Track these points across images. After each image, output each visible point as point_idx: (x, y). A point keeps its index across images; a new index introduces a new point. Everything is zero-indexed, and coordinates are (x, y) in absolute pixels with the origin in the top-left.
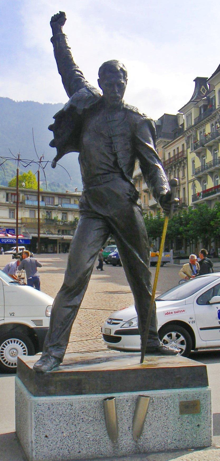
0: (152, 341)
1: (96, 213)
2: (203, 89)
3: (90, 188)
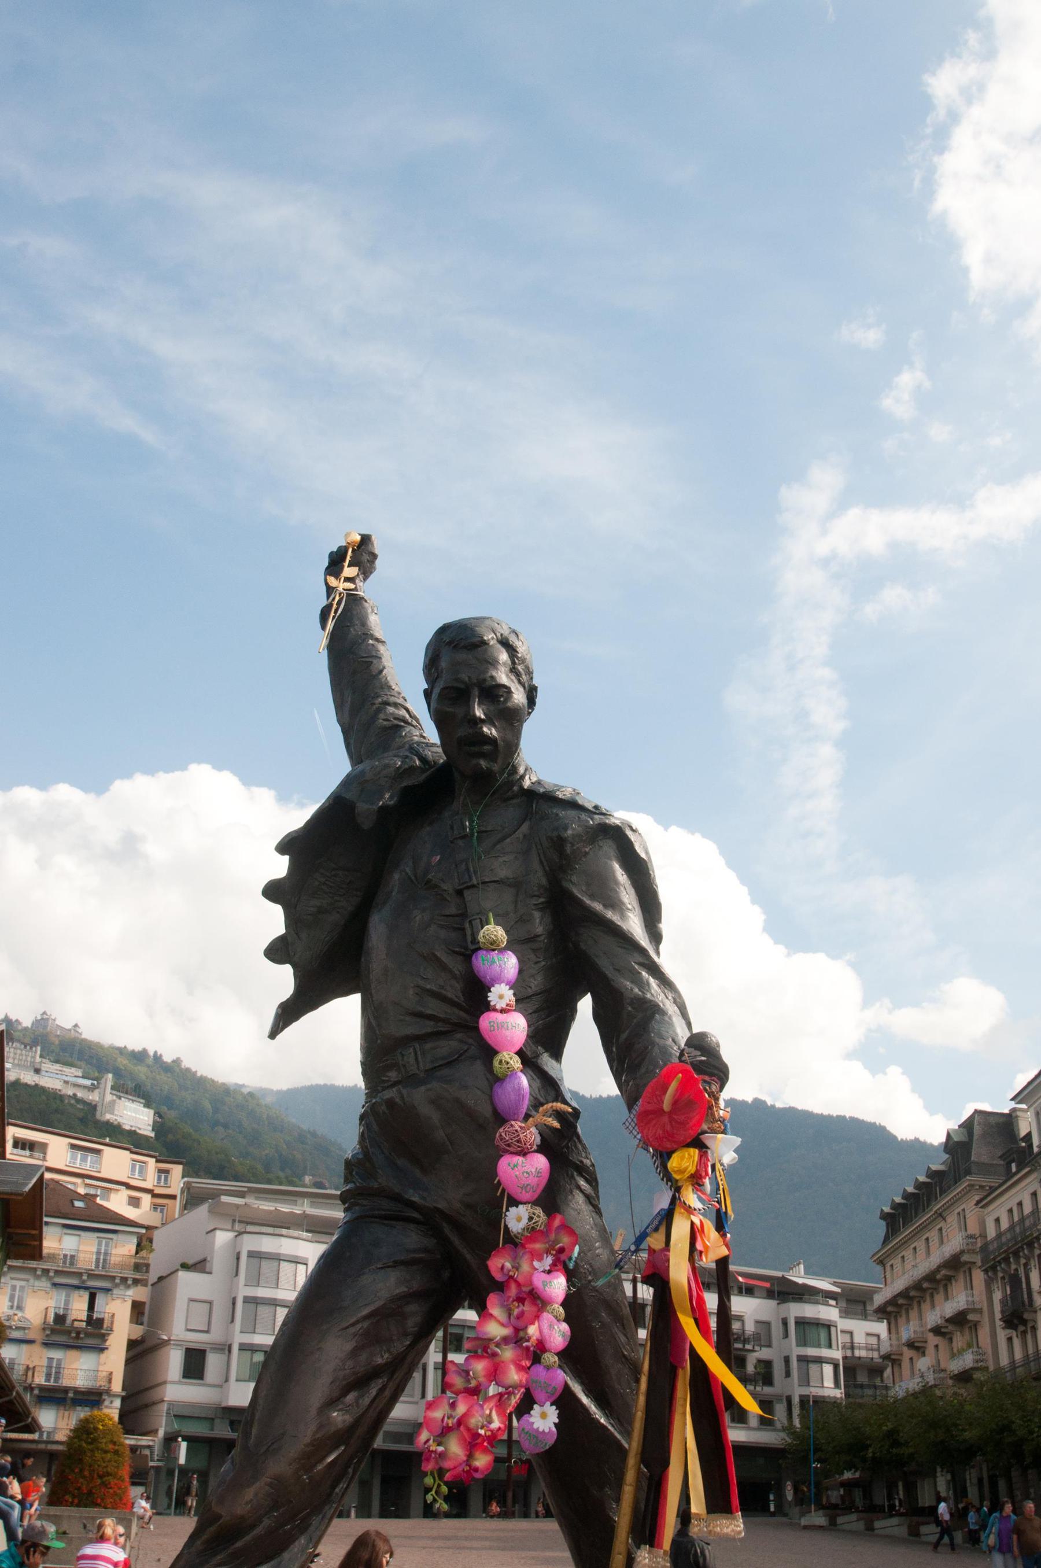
1: (397, 1198)
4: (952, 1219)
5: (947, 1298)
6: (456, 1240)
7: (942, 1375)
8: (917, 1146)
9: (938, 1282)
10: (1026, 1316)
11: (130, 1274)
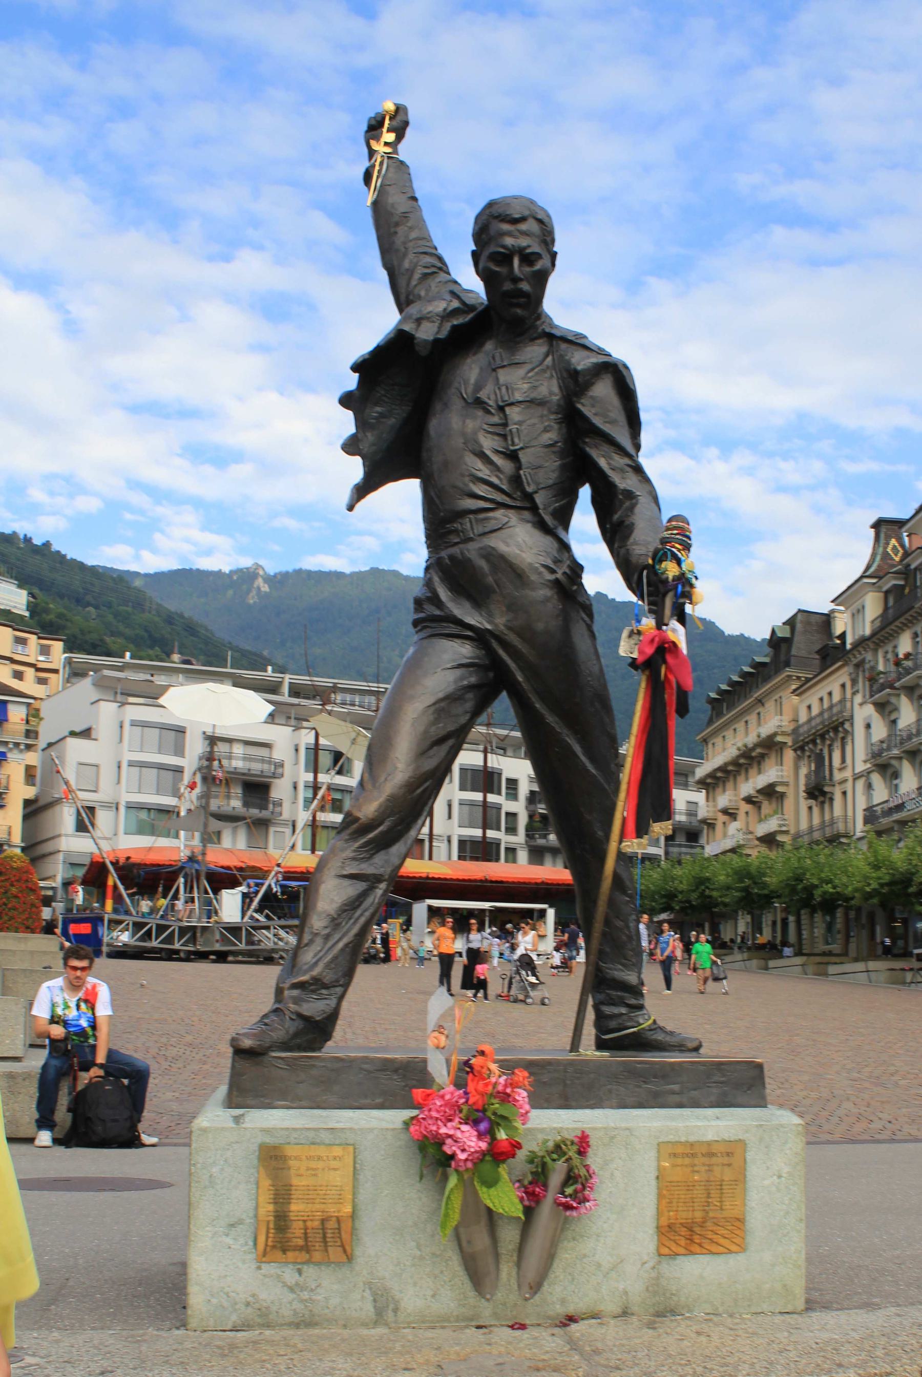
0: (623, 1010)
2: (894, 547)
3: (444, 554)
4: (770, 705)
5: (759, 772)
6: (501, 652)
7: (750, 836)
8: (741, 640)
9: (752, 758)
10: (826, 789)
11: (22, 740)
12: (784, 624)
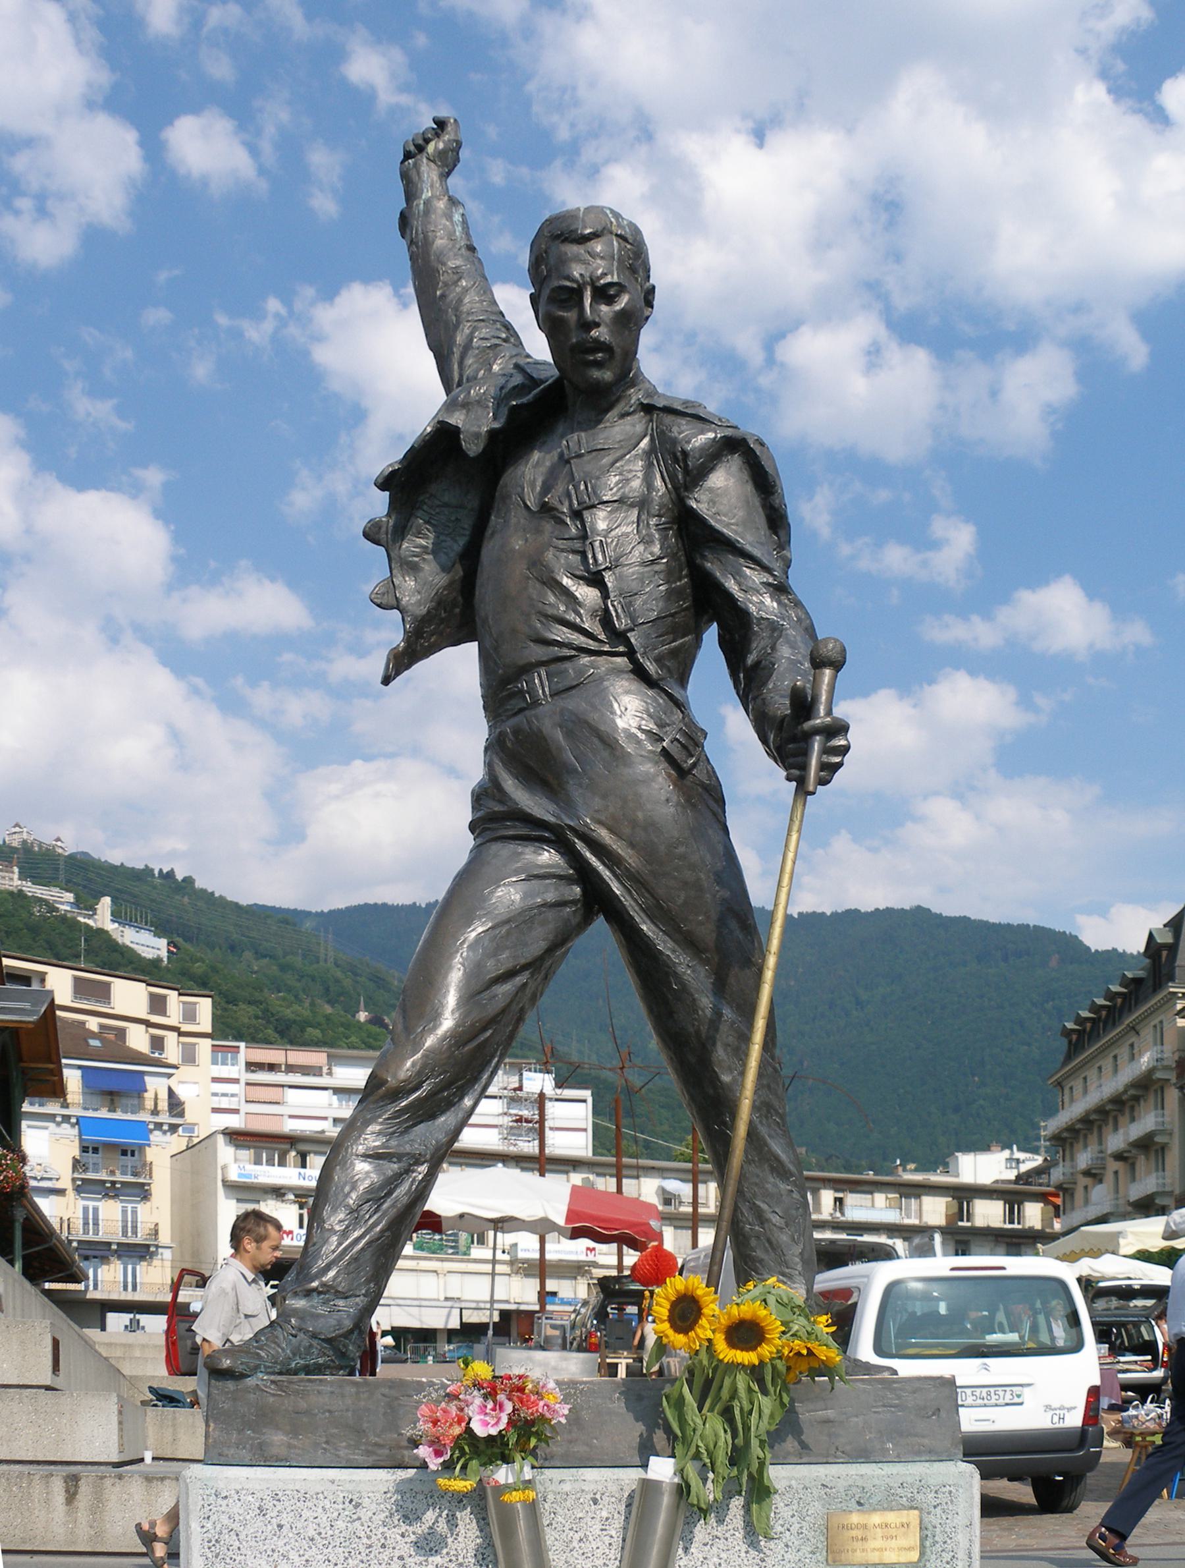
4: (1147, 1033)
5: (1133, 1119)
6: (593, 860)
8: (1113, 957)
12: (1165, 926)
